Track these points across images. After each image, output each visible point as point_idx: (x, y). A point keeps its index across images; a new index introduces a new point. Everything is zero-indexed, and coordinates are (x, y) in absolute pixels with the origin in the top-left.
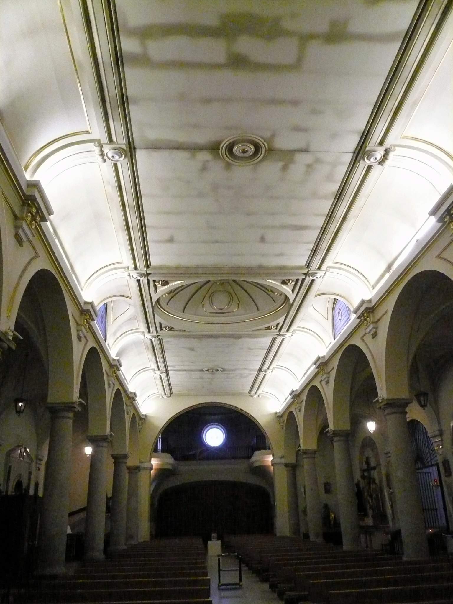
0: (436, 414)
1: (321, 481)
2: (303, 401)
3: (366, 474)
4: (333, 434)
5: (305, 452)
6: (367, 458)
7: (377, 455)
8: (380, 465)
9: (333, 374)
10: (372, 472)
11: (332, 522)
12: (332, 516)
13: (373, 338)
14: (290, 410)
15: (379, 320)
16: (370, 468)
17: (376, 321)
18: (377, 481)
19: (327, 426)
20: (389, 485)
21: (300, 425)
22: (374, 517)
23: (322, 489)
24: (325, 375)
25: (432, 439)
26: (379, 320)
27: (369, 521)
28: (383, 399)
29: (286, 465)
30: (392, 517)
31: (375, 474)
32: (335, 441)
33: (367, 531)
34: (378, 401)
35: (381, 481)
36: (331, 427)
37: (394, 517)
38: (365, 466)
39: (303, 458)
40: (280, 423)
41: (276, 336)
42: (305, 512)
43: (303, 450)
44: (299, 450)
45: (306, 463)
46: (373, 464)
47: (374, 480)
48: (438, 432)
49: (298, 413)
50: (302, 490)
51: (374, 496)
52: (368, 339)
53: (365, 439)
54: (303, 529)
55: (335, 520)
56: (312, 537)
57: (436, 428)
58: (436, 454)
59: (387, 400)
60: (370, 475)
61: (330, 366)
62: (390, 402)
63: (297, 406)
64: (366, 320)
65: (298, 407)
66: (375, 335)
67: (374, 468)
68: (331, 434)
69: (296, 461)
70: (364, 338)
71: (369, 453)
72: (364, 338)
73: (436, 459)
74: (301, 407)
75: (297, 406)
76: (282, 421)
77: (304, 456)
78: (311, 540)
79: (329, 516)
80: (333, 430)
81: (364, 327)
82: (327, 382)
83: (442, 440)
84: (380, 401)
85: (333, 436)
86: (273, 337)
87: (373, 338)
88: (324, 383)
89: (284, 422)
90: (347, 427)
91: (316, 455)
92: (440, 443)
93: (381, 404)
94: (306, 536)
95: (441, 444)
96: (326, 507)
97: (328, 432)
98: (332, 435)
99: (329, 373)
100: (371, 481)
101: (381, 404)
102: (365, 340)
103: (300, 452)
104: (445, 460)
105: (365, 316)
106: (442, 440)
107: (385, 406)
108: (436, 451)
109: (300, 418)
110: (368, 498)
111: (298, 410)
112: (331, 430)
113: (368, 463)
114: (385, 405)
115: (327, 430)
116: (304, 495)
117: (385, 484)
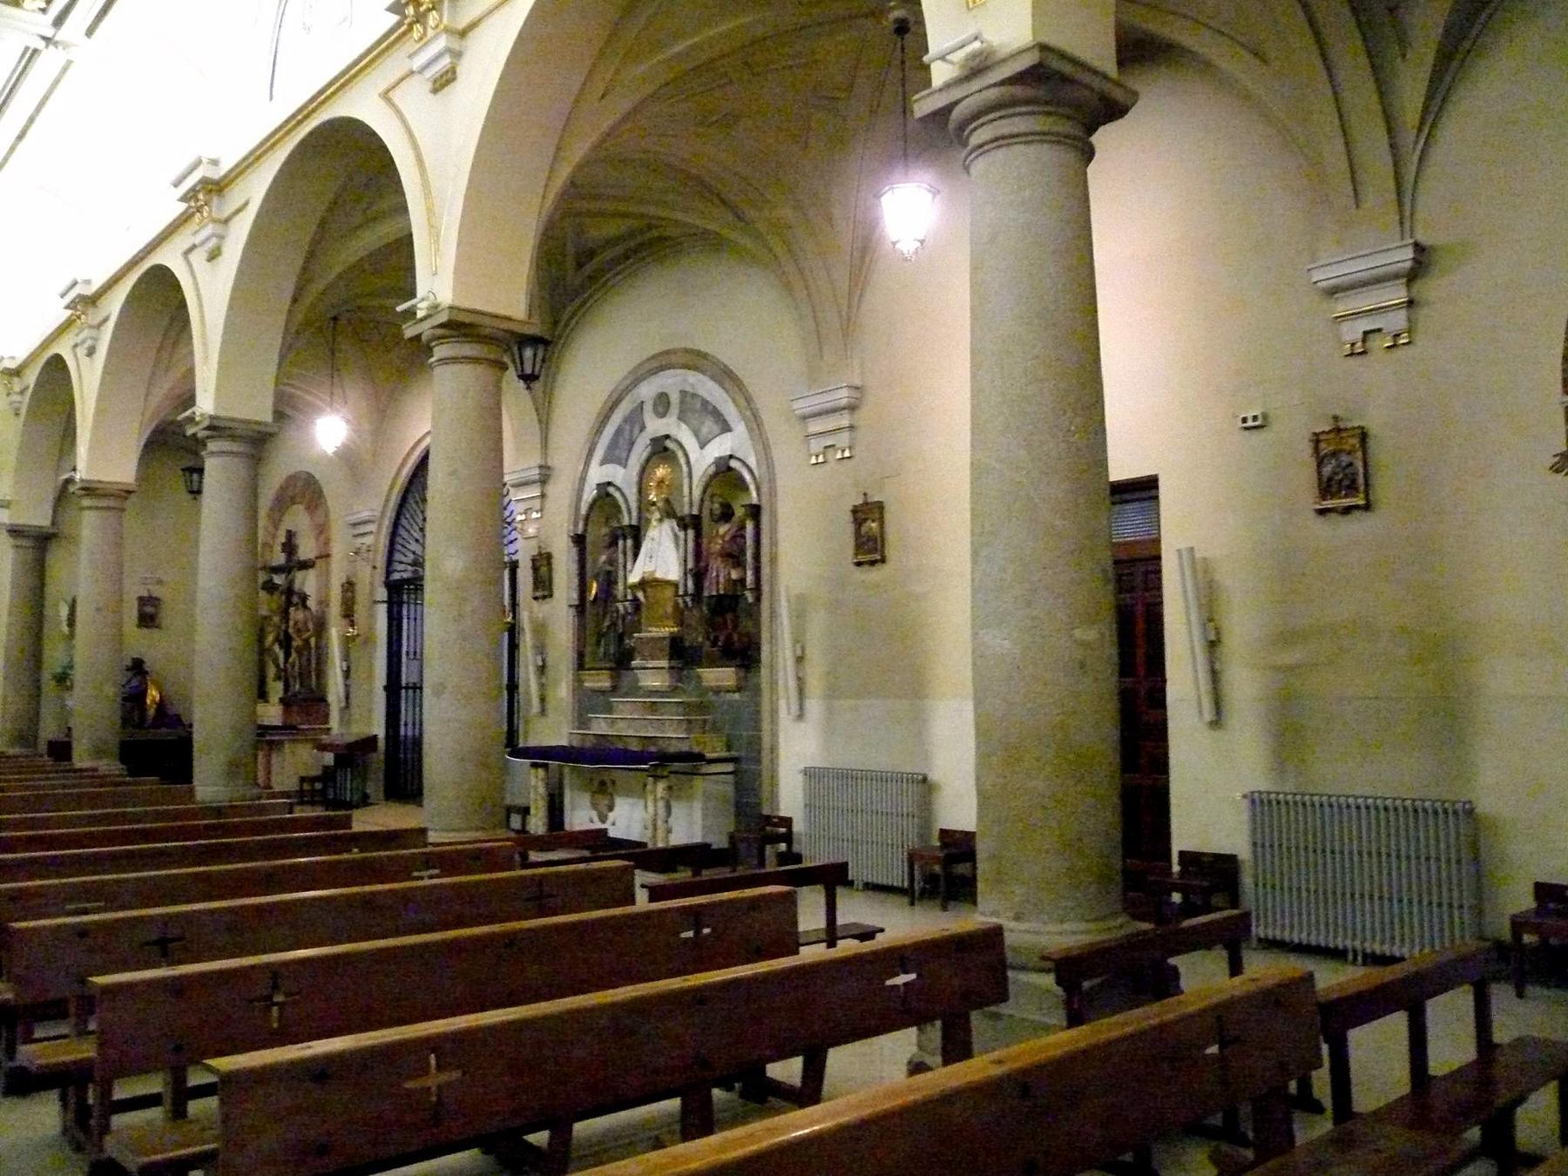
0: (540, 421)
1: (134, 591)
2: (106, 320)
3: (279, 580)
4: (208, 428)
5: (90, 490)
6: (290, 535)
7: (322, 530)
8: (328, 556)
9: (241, 229)
10: (299, 576)
11: (151, 712)
12: (153, 694)
13: (435, 91)
14: (55, 349)
15: (473, 25)
16: (295, 564)
17: (461, 25)
18: (311, 603)
19: (189, 400)
20: (348, 614)
21: (83, 403)
22: (286, 702)
23: (131, 613)
24: (211, 226)
25: (512, 490)
26: (473, 25)
27: (272, 713)
28: (435, 309)
29: (15, 532)
30: (343, 704)
31: (308, 582)
32: (212, 453)
33: (266, 739)
34: (411, 313)
35: (324, 603)
36: (206, 404)
37: (347, 706)
38: (279, 558)
39: (83, 509)
40: (8, 394)
41: (41, 44)
42: (63, 679)
43: (82, 480)
44: (69, 481)
45: (89, 525)
46: (306, 550)
47: (304, 598)
48: (537, 471)
49: (84, 360)
50: (64, 612)
51: (297, 643)
52: (414, 96)
53: (292, 479)
54: (49, 730)
55: (161, 706)
56: (81, 758)
57: (536, 460)
58: (514, 535)
59: (451, 308)
60: (291, 583)
61: (235, 197)
62: (462, 318)
63: (82, 336)
64: (199, 210)
65: (83, 342)
66: (214, 255)
67: (306, 565)
68: (201, 426)
69: (53, 523)
70: (396, 96)
71: (298, 519)
72: (396, 96)
73: (512, 548)
74: (96, 339)
75: (82, 336)
76: (17, 388)
77: (86, 502)
78: (78, 764)
79: (144, 693)
80: (212, 413)
81: (409, 46)
82: (91, 352)
83: (543, 496)
84: (420, 314)
85: (208, 437)
86: (27, 49)
87: (435, 91)
88: (198, 258)
89: (22, 392)
90: (260, 410)
91: (128, 504)
92: (537, 504)
93: (426, 325)
94: (61, 750)
95: (538, 507)
96: (138, 667)
97: (191, 420)
98: (207, 433)
99: (226, 221)
100: (295, 599)
101: (426, 325)
102: (396, 101)
103: (72, 489)
104: (540, 554)
105: (198, 200)
106: (543, 496)
107: (440, 332)
108: (519, 526)
109: (87, 379)
110: (276, 648)
111: (81, 351)
112: (202, 415)
113: (290, 547)
114: (442, 326)
115: (188, 413)
116: (66, 629)
117: (335, 610)
